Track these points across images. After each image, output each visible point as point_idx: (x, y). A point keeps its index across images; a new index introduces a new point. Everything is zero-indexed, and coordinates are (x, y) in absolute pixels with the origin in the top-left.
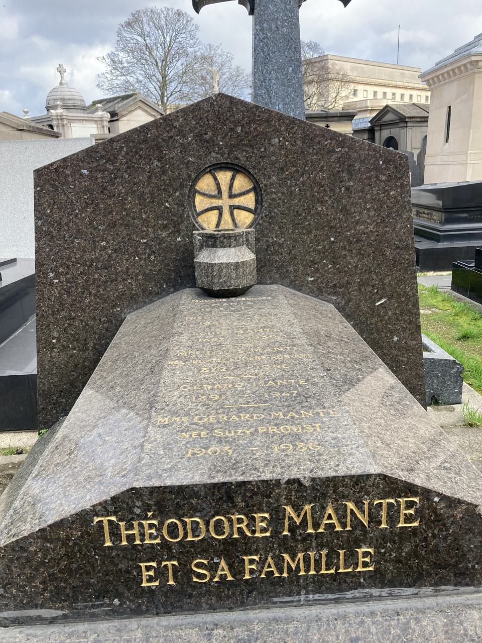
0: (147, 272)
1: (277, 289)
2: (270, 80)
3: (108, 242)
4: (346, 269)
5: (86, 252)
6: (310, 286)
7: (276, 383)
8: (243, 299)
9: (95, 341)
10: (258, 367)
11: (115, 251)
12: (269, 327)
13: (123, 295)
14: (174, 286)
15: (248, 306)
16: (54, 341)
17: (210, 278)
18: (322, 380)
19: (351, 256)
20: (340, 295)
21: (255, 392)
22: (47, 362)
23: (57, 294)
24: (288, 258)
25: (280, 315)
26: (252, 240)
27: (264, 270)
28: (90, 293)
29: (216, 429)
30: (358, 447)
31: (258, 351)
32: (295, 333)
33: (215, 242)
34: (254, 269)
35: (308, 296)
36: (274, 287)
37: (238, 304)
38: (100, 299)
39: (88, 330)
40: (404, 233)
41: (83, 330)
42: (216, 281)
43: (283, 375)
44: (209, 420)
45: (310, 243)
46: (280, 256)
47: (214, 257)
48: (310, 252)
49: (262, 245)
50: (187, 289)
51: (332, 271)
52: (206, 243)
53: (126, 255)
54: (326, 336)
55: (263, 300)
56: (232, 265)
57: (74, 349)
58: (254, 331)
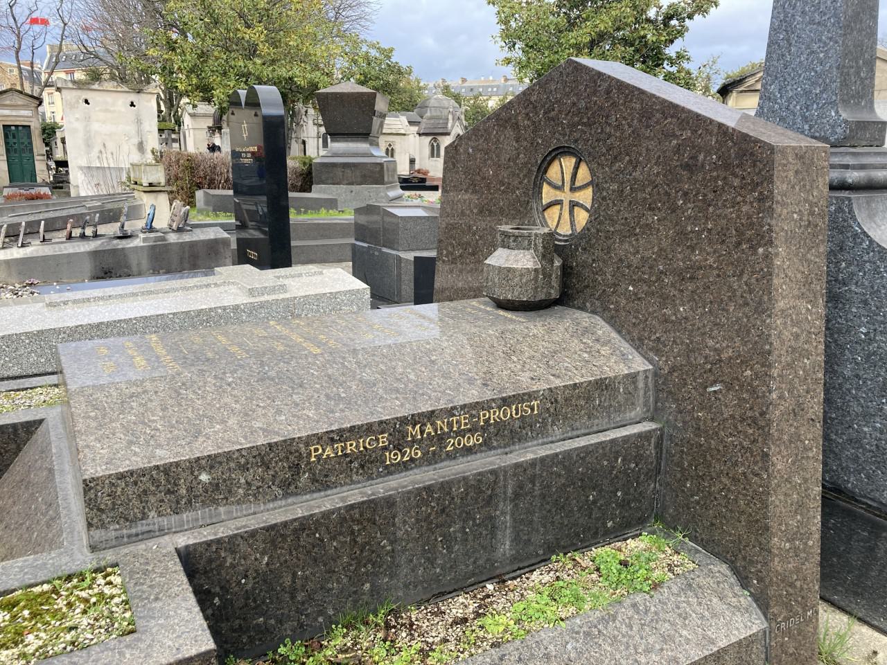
2: (793, 15)
40: (757, 280)
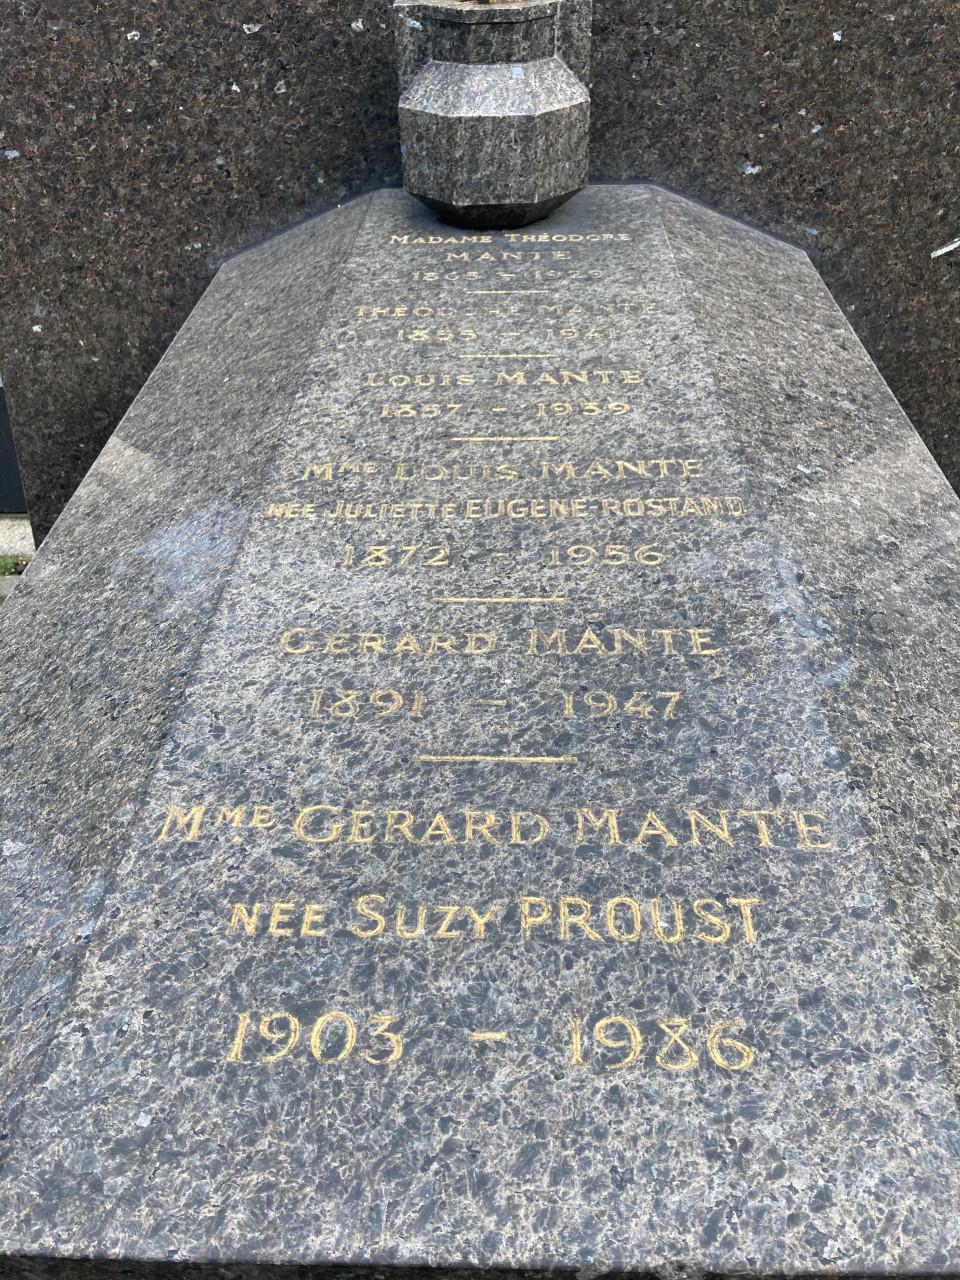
0: (270, 133)
1: (648, 202)
3: (145, 33)
4: (865, 139)
5: (83, 63)
6: (749, 192)
7: (608, 641)
8: (544, 238)
9: (144, 334)
10: (555, 553)
11: (170, 62)
12: (609, 364)
13: (204, 202)
14: (346, 181)
15: (555, 266)
16: (37, 328)
17: (442, 168)
18: (772, 637)
19: (886, 96)
20: (831, 222)
21: (532, 685)
22: (28, 384)
23: (22, 195)
24: (690, 97)
25: (647, 313)
26: (583, 37)
27: (615, 137)
28: (115, 195)
29: (364, 890)
30: (906, 1073)
31: (565, 472)
32: (691, 395)
33: (462, 40)
34: (581, 138)
35: (738, 224)
36: (639, 193)
37: (524, 260)
38: (145, 214)
39: (123, 303)
41: (109, 300)
42: (461, 177)
43: (634, 601)
44: (346, 832)
45: (766, 48)
46: (667, 92)
47: (457, 95)
48: (760, 79)
49: (615, 53)
50: (385, 192)
51: (820, 146)
52: (435, 44)
53: (202, 75)
54: (789, 397)
55: (601, 243)
56: (511, 126)
57: (94, 352)
58: (560, 379)
